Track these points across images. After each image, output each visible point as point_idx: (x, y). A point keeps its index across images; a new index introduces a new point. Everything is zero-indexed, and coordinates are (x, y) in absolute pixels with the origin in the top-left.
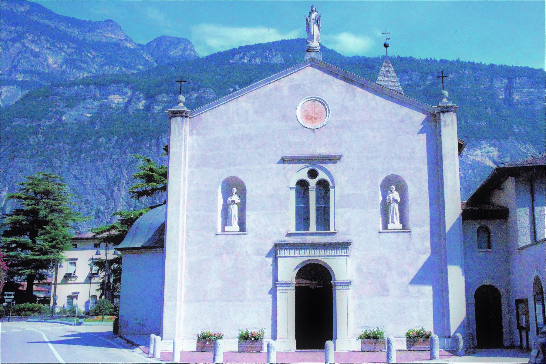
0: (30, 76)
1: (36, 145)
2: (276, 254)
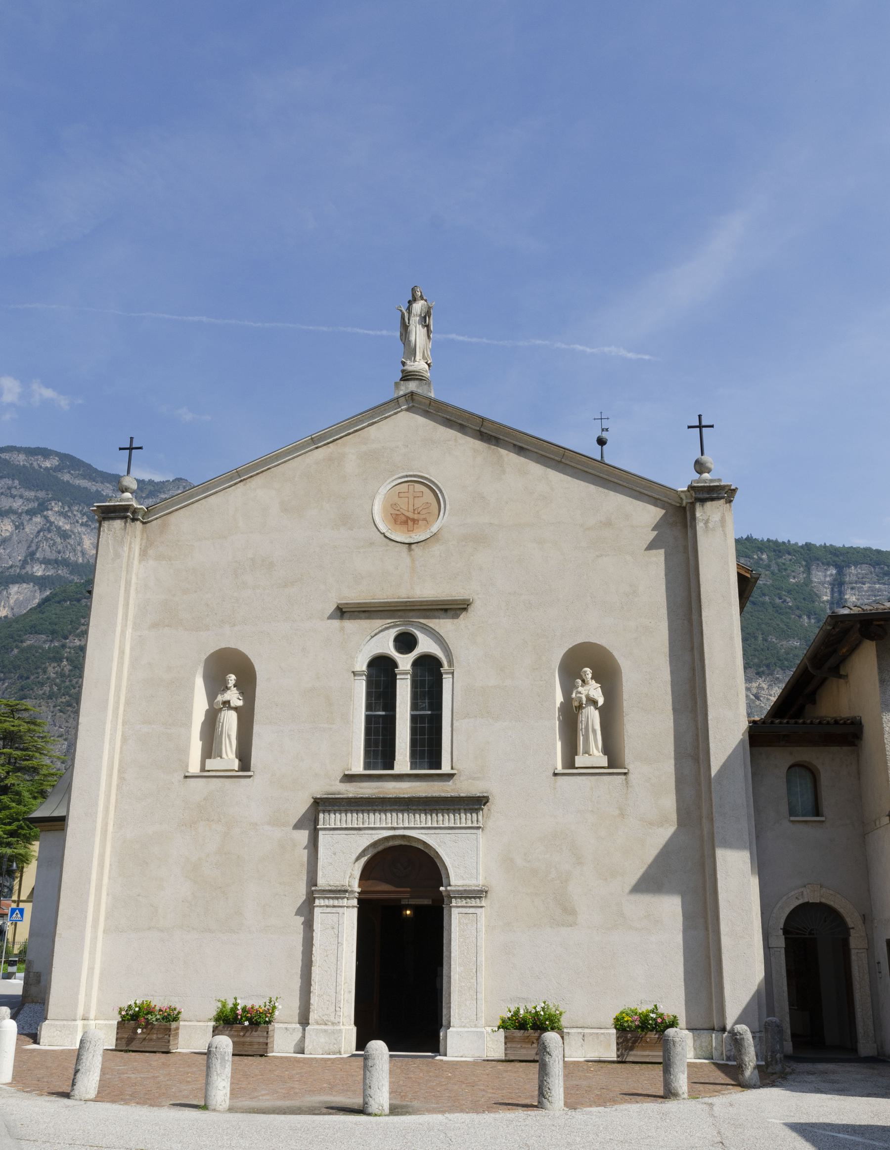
0: (54, 568)
1: (57, 678)
2: (316, 821)
